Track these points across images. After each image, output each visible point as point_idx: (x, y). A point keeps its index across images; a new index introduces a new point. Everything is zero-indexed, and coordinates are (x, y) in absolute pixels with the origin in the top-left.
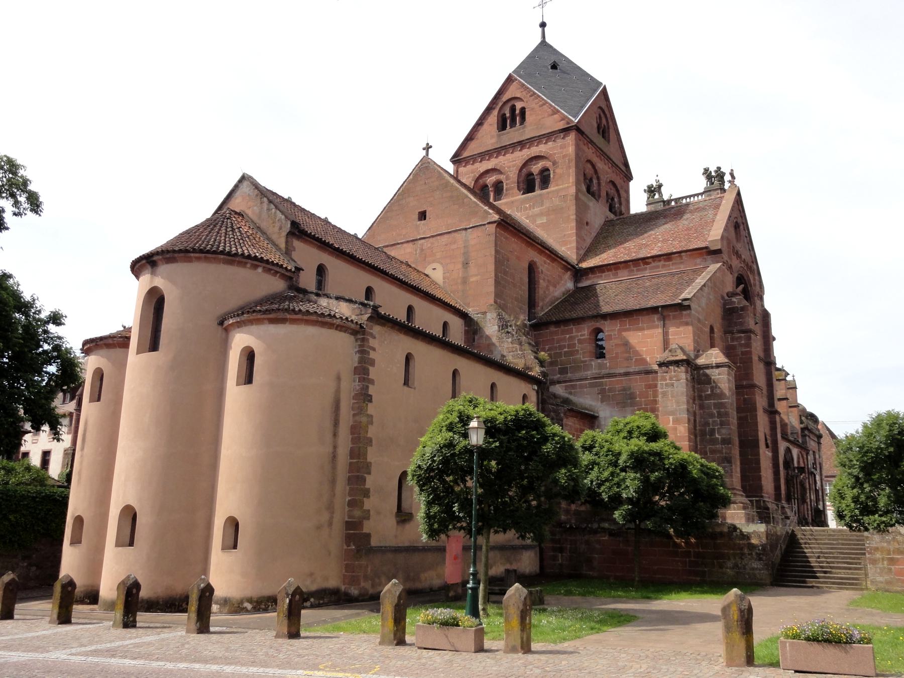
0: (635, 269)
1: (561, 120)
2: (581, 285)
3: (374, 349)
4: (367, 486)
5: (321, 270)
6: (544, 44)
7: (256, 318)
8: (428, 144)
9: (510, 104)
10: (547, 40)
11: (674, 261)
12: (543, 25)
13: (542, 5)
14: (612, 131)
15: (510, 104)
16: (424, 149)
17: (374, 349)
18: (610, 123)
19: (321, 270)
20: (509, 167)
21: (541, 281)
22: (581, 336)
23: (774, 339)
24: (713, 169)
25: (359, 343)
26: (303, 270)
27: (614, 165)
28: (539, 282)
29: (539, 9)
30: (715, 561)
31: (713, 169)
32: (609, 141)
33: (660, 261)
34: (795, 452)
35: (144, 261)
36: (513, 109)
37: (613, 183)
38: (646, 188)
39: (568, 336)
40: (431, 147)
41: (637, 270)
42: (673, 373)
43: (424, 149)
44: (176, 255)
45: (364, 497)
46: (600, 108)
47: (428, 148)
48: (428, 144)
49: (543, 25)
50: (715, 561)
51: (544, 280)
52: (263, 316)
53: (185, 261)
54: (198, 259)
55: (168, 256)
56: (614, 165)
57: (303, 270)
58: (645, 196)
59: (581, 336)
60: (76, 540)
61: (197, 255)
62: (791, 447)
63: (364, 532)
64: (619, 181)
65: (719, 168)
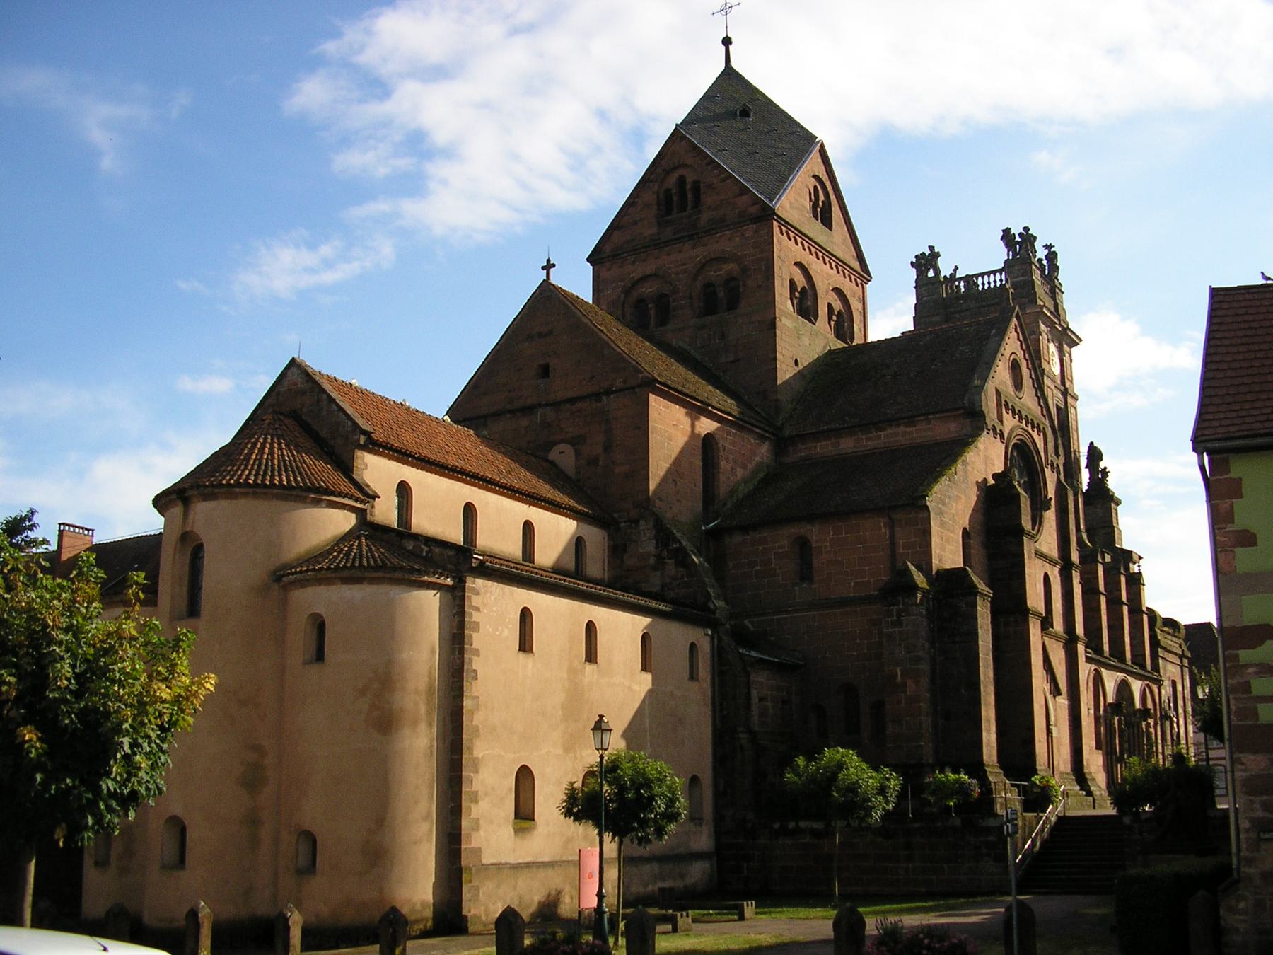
0: (864, 437)
1: (754, 205)
2: (790, 458)
3: (478, 609)
4: (474, 789)
5: (404, 490)
6: (729, 76)
7: (324, 576)
8: (548, 261)
9: (675, 175)
10: (734, 64)
11: (918, 427)
12: (727, 42)
13: (726, 9)
14: (835, 209)
15: (675, 175)
16: (543, 268)
17: (478, 609)
18: (833, 198)
19: (404, 490)
20: (677, 274)
21: (723, 464)
22: (779, 548)
23: (1118, 503)
24: (1016, 230)
25: (458, 603)
26: (379, 497)
27: (840, 264)
28: (718, 464)
29: (721, 17)
30: (945, 866)
31: (1016, 230)
32: (829, 226)
33: (899, 425)
34: (1136, 686)
35: (174, 496)
36: (682, 180)
37: (838, 291)
38: (914, 260)
39: (760, 548)
40: (554, 266)
41: (866, 438)
42: (901, 606)
43: (543, 268)
44: (216, 490)
45: (471, 802)
46: (816, 177)
47: (549, 266)
48: (548, 261)
49: (727, 42)
50: (945, 866)
51: (727, 459)
52: (333, 575)
53: (227, 498)
54: (245, 495)
55: (206, 491)
56: (840, 264)
57: (379, 497)
58: (913, 273)
59: (779, 548)
60: (102, 863)
61: (243, 490)
62: (1130, 679)
63: (473, 846)
64: (848, 287)
65: (1026, 229)
